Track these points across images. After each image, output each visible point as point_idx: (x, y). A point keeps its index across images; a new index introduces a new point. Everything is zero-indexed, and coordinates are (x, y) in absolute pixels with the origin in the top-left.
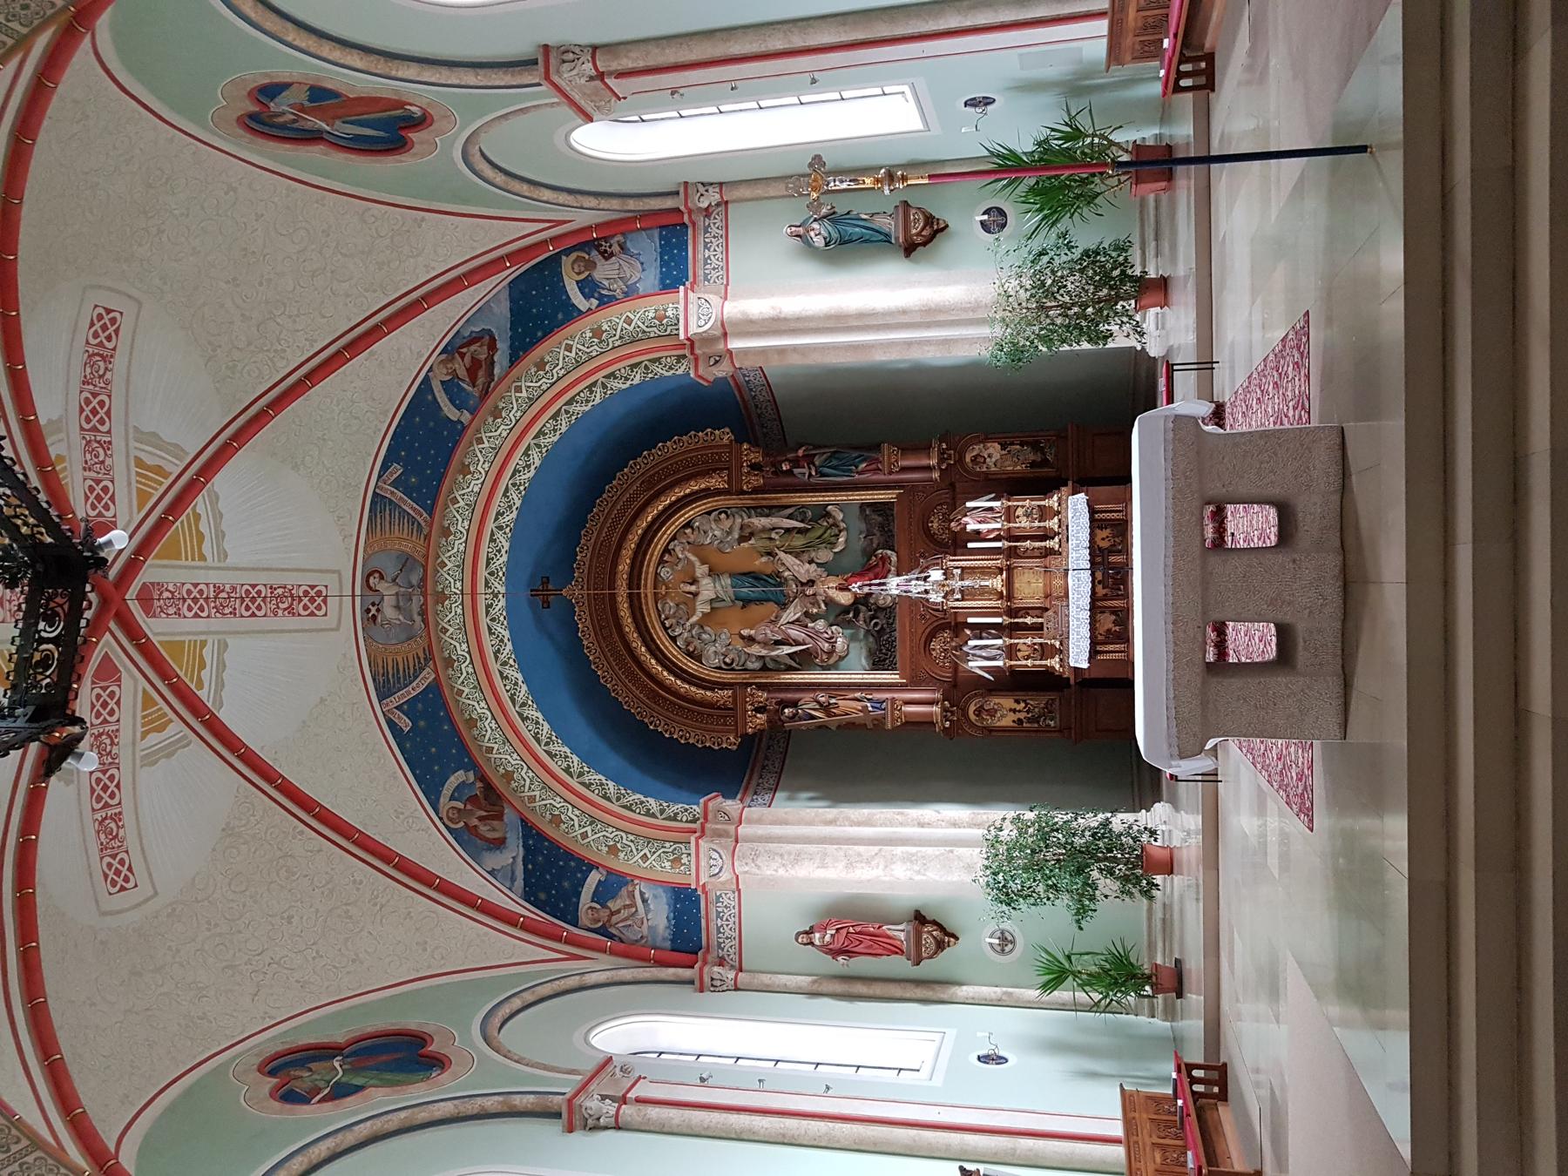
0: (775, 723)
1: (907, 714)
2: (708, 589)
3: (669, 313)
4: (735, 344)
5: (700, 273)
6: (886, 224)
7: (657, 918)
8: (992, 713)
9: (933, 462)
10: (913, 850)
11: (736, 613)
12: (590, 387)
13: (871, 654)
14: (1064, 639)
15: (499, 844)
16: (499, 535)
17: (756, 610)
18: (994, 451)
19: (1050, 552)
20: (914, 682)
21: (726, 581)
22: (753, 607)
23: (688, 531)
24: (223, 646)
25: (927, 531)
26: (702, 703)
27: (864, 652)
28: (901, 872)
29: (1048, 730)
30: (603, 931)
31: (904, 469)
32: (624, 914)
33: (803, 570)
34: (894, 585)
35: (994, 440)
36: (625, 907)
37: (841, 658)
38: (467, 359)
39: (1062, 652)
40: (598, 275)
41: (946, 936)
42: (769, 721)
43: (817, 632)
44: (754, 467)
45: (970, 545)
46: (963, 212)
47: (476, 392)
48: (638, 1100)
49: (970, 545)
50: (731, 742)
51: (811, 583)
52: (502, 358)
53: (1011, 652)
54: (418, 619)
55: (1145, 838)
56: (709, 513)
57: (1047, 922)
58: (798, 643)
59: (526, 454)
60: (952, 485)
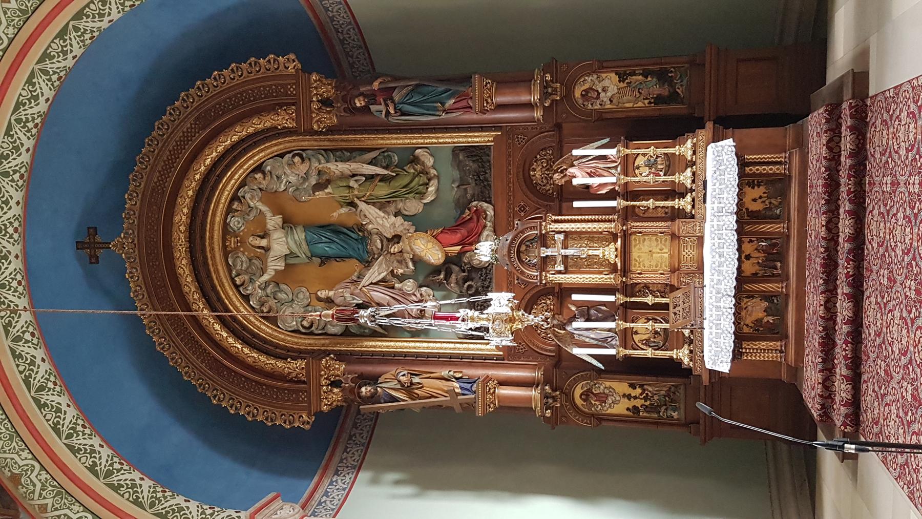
0: (353, 399)
1: (501, 398)
2: (280, 244)
8: (602, 398)
9: (535, 97)
11: (314, 270)
14: (697, 330)
17: (337, 267)
19: (675, 215)
21: (300, 235)
23: (259, 176)
29: (671, 423)
39: (694, 342)
44: (326, 102)
49: (576, 204)
50: (303, 420)
53: (626, 337)
56: (282, 156)
60: (558, 127)
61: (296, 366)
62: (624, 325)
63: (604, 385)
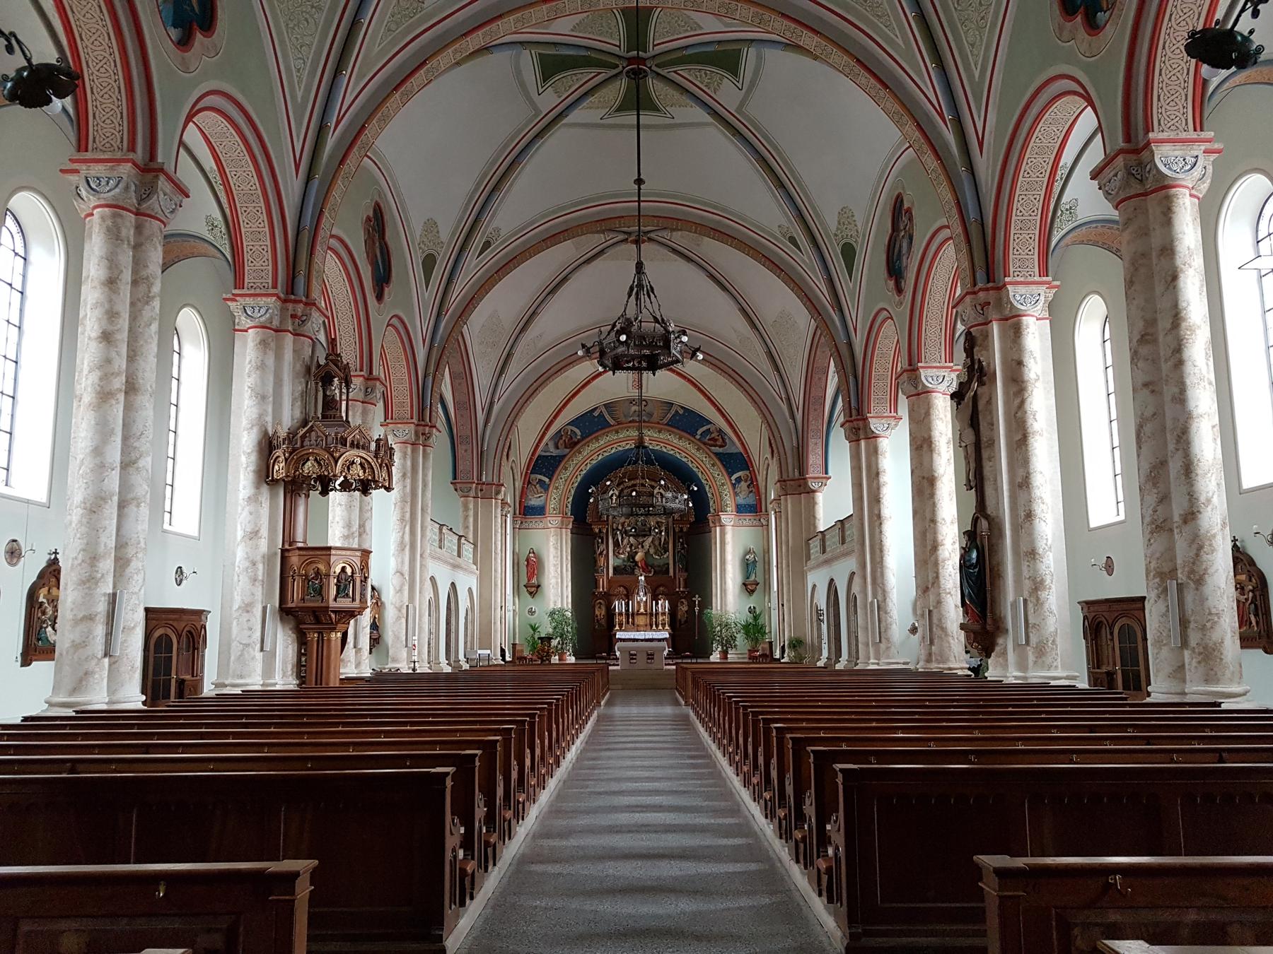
0: (595, 536)
6: (753, 578)
7: (534, 501)
15: (557, 448)
18: (685, 608)
20: (609, 581)
28: (553, 581)
39: (621, 630)
41: (532, 594)
46: (752, 602)
53: (620, 614)
63: (603, 608)
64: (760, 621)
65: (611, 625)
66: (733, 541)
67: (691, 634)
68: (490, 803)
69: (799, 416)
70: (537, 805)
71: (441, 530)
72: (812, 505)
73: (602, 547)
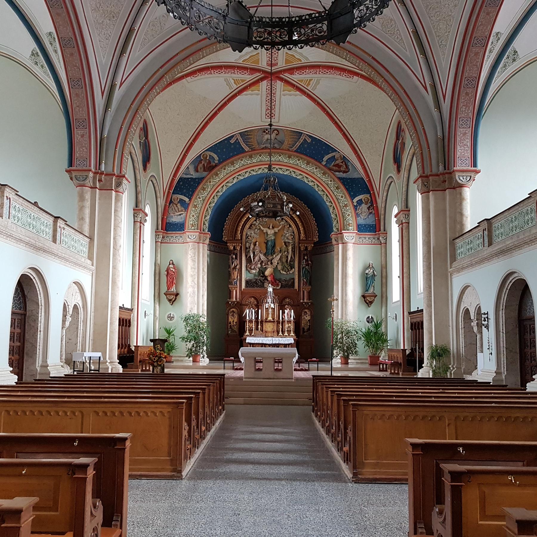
0: (229, 253)
1: (233, 291)
3: (350, 227)
4: (340, 246)
5: (362, 236)
6: (371, 291)
7: (175, 218)
8: (233, 315)
9: (305, 301)
10: (196, 293)
11: (263, 240)
12: (331, 202)
13: (250, 280)
15: (196, 170)
16: (288, 172)
17: (264, 246)
18: (308, 318)
19: (278, 333)
20: (242, 293)
22: (265, 245)
24: (258, 95)
25: (284, 298)
26: (237, 230)
27: (251, 278)
28: (190, 290)
30: (171, 202)
31: (304, 292)
32: (176, 208)
33: (275, 261)
34: (270, 289)
35: (311, 317)
36: (178, 209)
37: (249, 271)
38: (341, 164)
39: (250, 335)
40: (363, 205)
41: (172, 302)
42: (231, 251)
43: (256, 265)
44: (306, 248)
45: (281, 311)
46: (370, 312)
47: (331, 166)
48: (140, 226)
49: (281, 311)
51: (272, 263)
52: (341, 175)
53: (251, 321)
54: (264, 146)
55: (202, 356)
56: (293, 233)
57: (181, 330)
58: (254, 259)
59: (312, 181)
60: (299, 306)
61: (239, 235)
62: (254, 321)
63: (236, 316)
64: (383, 329)
65: (242, 330)
66: (354, 257)
67: (313, 341)
68: (197, 419)
69: (446, 106)
70: (205, 440)
71: (55, 222)
72: (459, 201)
73: (236, 262)
